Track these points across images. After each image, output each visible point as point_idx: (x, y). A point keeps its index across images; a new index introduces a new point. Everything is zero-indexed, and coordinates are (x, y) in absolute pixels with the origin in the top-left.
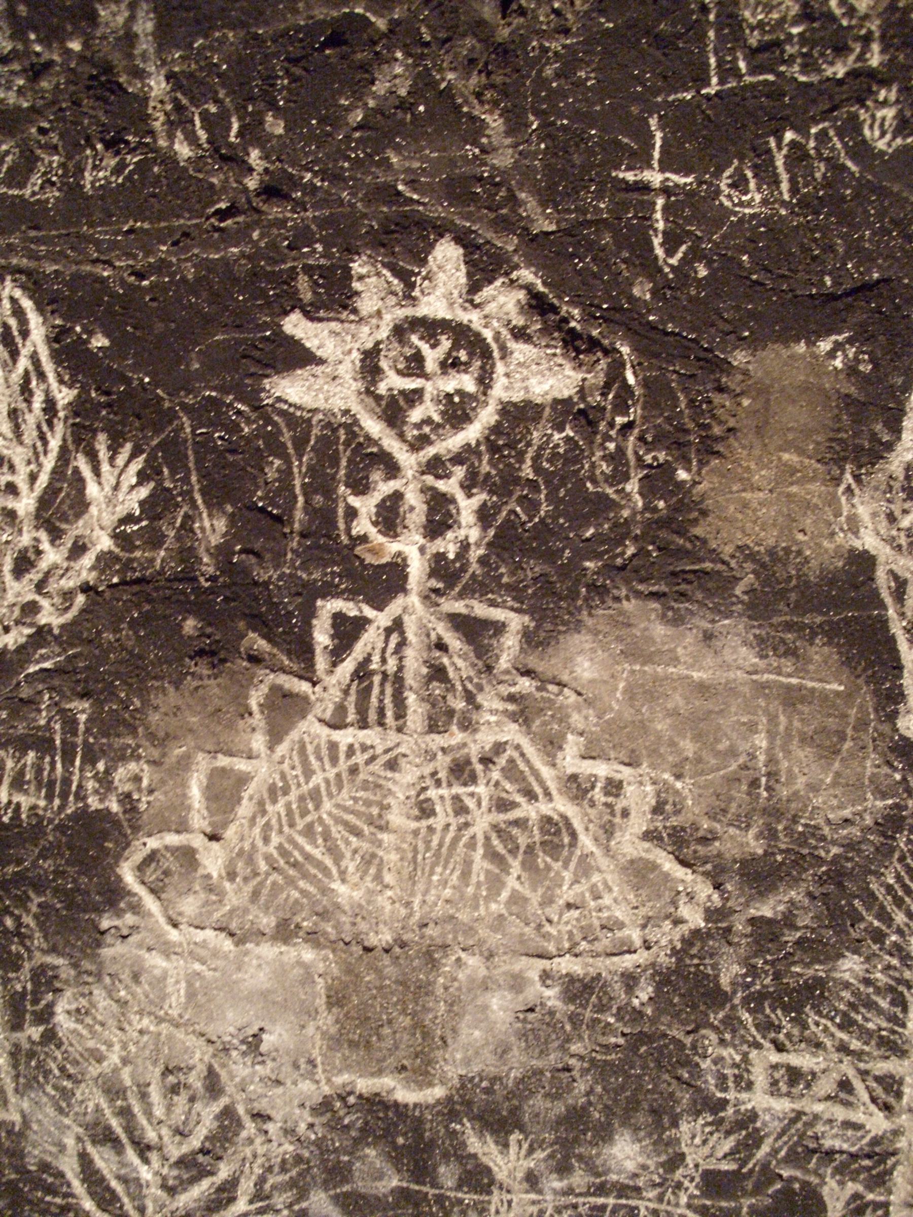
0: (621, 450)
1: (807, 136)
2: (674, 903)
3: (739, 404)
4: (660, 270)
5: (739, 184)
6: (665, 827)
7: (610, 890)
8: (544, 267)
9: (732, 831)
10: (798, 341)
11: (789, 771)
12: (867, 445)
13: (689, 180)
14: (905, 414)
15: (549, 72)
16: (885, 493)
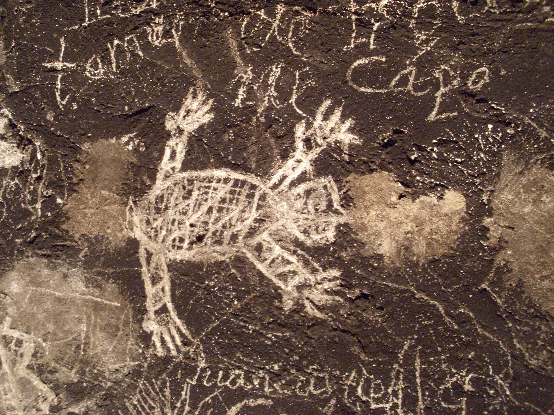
0: (35, 190)
1: (123, 41)
2: (36, 400)
3: (85, 168)
4: (58, 107)
5: (95, 66)
6: (36, 364)
7: (11, 391)
8: (11, 108)
9: (64, 369)
10: (113, 137)
11: (94, 343)
12: (139, 186)
13: (72, 65)
14: (158, 171)
15: (21, 21)
16: (146, 210)
